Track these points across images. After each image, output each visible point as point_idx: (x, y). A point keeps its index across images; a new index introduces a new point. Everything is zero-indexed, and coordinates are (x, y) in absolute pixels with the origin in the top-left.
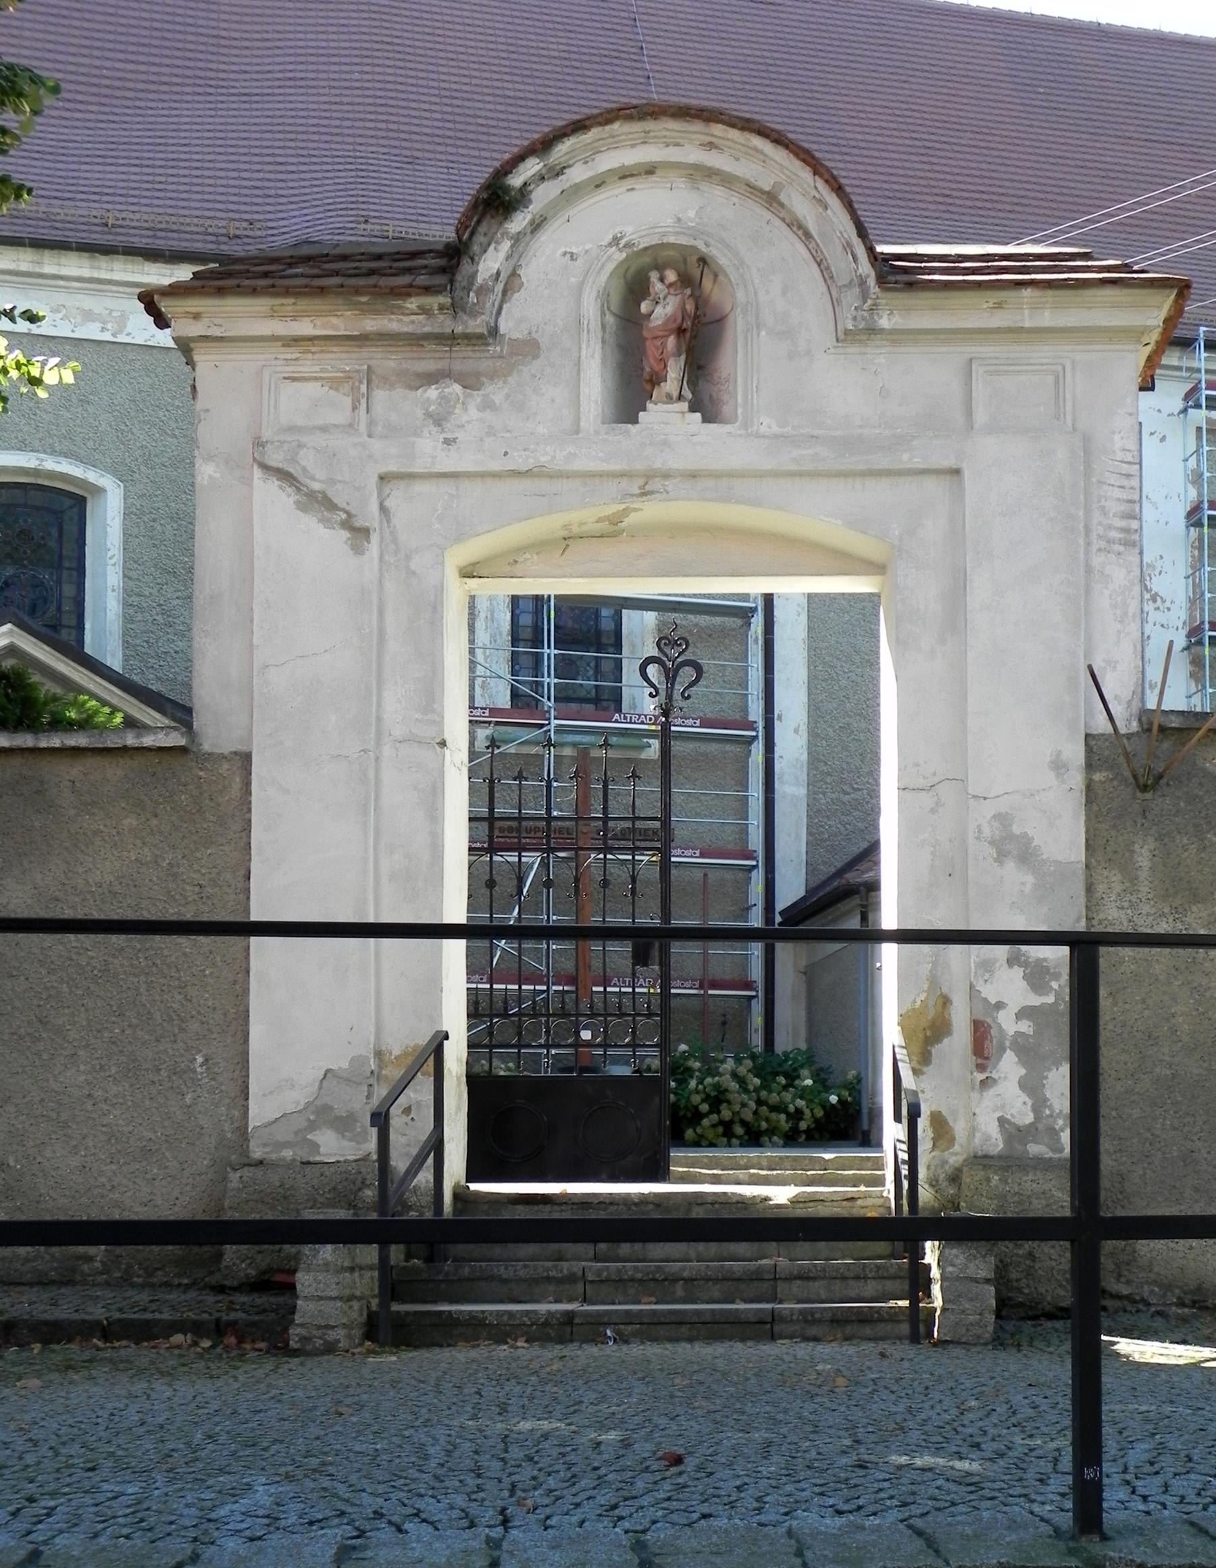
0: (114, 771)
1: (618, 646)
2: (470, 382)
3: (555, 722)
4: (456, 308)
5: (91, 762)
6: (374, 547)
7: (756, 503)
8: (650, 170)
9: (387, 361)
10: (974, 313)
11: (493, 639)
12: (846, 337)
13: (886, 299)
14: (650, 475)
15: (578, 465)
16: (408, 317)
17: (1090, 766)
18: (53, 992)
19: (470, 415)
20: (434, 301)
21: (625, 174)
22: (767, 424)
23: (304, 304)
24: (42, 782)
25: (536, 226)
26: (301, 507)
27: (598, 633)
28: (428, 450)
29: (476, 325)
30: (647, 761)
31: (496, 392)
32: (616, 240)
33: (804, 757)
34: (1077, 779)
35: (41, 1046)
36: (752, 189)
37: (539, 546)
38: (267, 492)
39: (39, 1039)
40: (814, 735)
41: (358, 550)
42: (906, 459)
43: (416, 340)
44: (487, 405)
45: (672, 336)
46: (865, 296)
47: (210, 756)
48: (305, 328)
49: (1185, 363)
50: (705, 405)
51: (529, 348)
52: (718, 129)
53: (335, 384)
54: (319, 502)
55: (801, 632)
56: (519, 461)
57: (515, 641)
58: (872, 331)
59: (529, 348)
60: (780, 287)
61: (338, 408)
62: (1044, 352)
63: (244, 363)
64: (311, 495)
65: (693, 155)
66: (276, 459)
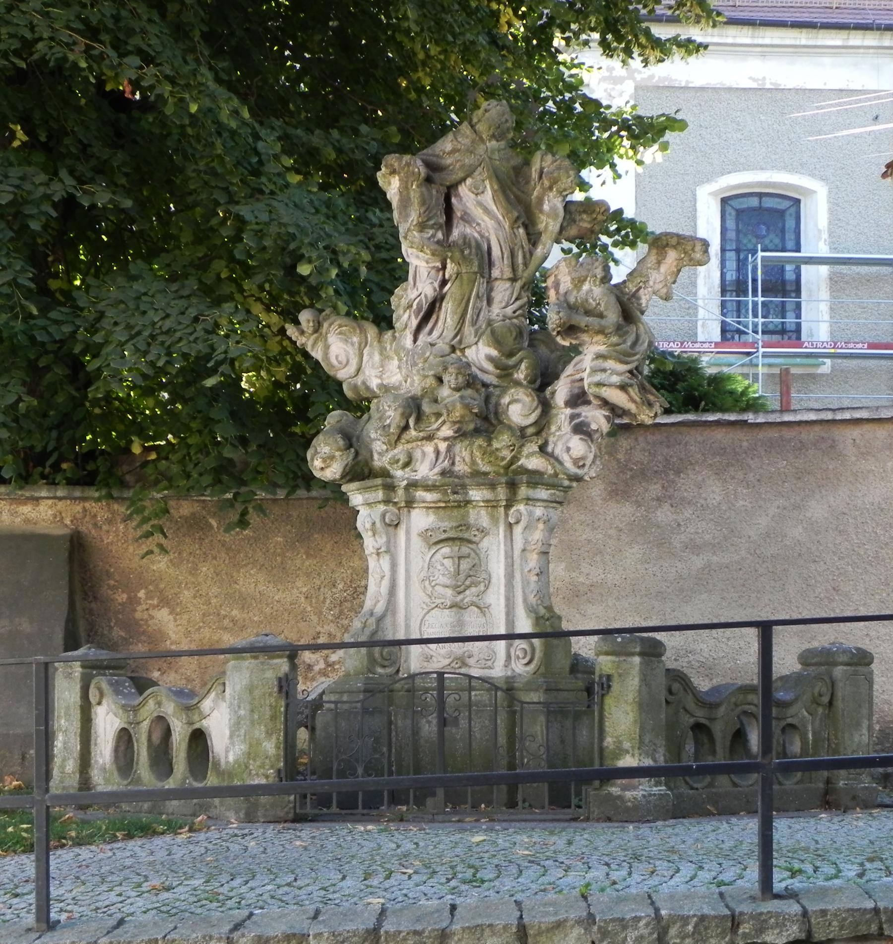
1: (798, 291)
3: (762, 350)
11: (709, 292)
18: (842, 571)
24: (834, 441)
27: (784, 282)
30: (822, 375)
35: (834, 604)
39: (833, 601)
57: (724, 292)
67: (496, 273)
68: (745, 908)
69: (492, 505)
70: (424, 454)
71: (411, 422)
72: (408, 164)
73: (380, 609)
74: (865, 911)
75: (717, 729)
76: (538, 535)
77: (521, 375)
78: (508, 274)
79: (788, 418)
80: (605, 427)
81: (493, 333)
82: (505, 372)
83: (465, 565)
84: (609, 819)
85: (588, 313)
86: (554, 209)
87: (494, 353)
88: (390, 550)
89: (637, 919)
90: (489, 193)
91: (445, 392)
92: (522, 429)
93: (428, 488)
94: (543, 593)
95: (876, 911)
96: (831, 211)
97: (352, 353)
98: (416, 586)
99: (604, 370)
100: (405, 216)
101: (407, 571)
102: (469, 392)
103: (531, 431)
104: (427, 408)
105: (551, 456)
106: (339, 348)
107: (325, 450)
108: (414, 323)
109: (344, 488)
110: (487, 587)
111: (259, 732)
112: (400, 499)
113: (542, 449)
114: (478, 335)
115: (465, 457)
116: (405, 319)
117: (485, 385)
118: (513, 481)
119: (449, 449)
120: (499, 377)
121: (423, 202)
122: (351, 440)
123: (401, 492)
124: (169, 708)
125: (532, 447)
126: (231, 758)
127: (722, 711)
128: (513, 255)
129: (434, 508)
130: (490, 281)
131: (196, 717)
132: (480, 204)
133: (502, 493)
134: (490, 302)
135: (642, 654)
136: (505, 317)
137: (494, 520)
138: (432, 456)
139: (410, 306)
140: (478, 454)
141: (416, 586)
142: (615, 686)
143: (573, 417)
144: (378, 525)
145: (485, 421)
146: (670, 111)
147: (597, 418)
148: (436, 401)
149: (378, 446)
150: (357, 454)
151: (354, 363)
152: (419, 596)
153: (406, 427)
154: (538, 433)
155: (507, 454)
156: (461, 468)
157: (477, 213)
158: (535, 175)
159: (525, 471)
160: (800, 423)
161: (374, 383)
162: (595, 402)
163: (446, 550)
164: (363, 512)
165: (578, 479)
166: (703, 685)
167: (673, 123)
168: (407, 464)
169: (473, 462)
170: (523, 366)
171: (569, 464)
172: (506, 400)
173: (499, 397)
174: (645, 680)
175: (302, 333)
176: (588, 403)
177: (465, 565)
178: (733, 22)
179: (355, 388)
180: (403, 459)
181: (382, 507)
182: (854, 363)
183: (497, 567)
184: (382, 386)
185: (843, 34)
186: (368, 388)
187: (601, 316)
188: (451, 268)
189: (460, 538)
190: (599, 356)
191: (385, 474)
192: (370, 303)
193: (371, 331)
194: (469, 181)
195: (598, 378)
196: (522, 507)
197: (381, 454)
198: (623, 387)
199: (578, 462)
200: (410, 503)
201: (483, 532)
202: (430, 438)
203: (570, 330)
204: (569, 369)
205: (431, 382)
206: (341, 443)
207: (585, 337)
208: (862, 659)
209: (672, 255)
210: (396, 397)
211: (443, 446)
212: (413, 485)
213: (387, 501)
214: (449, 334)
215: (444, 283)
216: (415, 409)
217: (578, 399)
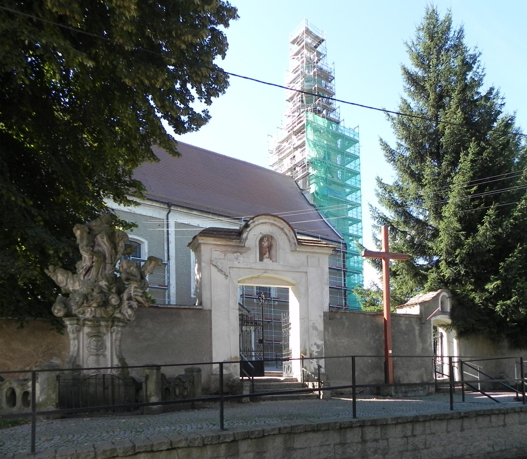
0: (191, 312)
2: (241, 253)
4: (240, 242)
5: (188, 310)
6: (228, 278)
7: (280, 275)
8: (265, 223)
9: (230, 249)
10: (309, 249)
12: (292, 251)
13: (298, 246)
14: (266, 270)
15: (257, 268)
16: (233, 243)
17: (324, 316)
19: (241, 259)
20: (238, 241)
21: (262, 223)
22: (281, 263)
23: (219, 239)
25: (250, 230)
26: (218, 271)
28: (236, 264)
29: (243, 245)
31: (244, 255)
32: (261, 233)
33: (175, 293)
34: (322, 318)
36: (280, 227)
37: (248, 279)
38: (213, 268)
40: (177, 289)
41: (226, 279)
42: (301, 270)
43: (234, 246)
44: (243, 257)
45: (266, 248)
46: (295, 245)
47: (205, 310)
48: (219, 243)
49: (239, 223)
50: (270, 257)
51: (249, 249)
52: (276, 218)
53: (222, 252)
54: (221, 271)
55: (174, 269)
56: (249, 266)
58: (296, 250)
59: (249, 249)
60: (283, 242)
61: (222, 256)
62: (317, 255)
63: (210, 247)
64: (219, 269)
65: (272, 221)
66: (214, 263)
67: (107, 261)
68: (219, 433)
69: (107, 326)
70: (88, 311)
71: (85, 302)
72: (83, 227)
73: (75, 354)
74: (245, 432)
75: (171, 389)
76: (119, 336)
77: (113, 291)
78: (110, 262)
79: (169, 306)
80: (137, 306)
81: (107, 278)
82: (110, 289)
83: (99, 343)
84: (149, 414)
85: (132, 275)
86: (122, 245)
87: (107, 284)
88: (78, 338)
89: (198, 438)
90: (105, 239)
91: (95, 294)
92: (115, 306)
93: (89, 321)
94: (120, 352)
95: (248, 432)
96: (149, 248)
97: (64, 279)
98: (85, 349)
99: (137, 291)
100: (82, 242)
101: (83, 344)
102: (101, 294)
103: (117, 306)
104: (90, 298)
105: (122, 314)
106: (60, 278)
107: (58, 307)
108: (84, 273)
109: (63, 319)
110: (106, 349)
111: (51, 392)
112: (81, 324)
113: (120, 311)
114: (103, 278)
115: (99, 313)
116: (81, 271)
117: (105, 293)
118: (113, 320)
119: (95, 310)
120: (108, 291)
121: (88, 239)
122: (66, 306)
123: (81, 321)
124: (15, 385)
125: (118, 311)
126: (40, 400)
127: (172, 384)
128: (111, 257)
129: (89, 327)
130: (105, 263)
131: (25, 388)
132: (103, 242)
133: (110, 323)
134: (105, 269)
135: (156, 369)
136: (109, 274)
137: (107, 331)
138: (90, 311)
139: (83, 268)
140: (102, 312)
141: (85, 349)
142: (150, 378)
143: (129, 303)
144: (75, 330)
145: (105, 303)
146: (134, 222)
147: (135, 304)
148: (92, 296)
149: (74, 308)
150: (68, 309)
151: (65, 282)
152: (86, 351)
153: (83, 303)
154: (118, 307)
155: (111, 313)
156: (98, 315)
157: (102, 244)
158: (117, 236)
159: (116, 318)
160: (171, 308)
161: (71, 289)
162: (134, 300)
163: (94, 339)
164: (69, 326)
165: (129, 320)
166: (167, 377)
167: (134, 225)
168: (83, 314)
169: (101, 314)
170: (114, 288)
171: (127, 316)
172: (111, 297)
173: (109, 296)
174: (157, 377)
175: (50, 272)
176: (132, 300)
177: (99, 343)
178: (148, 199)
179: (65, 290)
180: (82, 312)
181: (76, 326)
182: (155, 289)
183: (108, 344)
184: (73, 290)
185: (151, 202)
186: (69, 290)
187: (136, 276)
188: (95, 258)
189: (98, 336)
190: (135, 287)
191: (75, 316)
192: (70, 266)
193: (70, 274)
194: (100, 235)
195: (135, 293)
196: (115, 328)
197: (75, 310)
198: (142, 296)
199: (129, 316)
200: (84, 325)
201: (104, 334)
202: (89, 306)
203: (128, 279)
204: (127, 290)
205: (90, 290)
206: (63, 306)
207: (131, 282)
208: (199, 371)
209: (153, 263)
210: (79, 294)
211: (93, 309)
212: (85, 320)
213: (77, 324)
214: (94, 277)
215: (93, 262)
216: (86, 298)
217: (130, 299)
